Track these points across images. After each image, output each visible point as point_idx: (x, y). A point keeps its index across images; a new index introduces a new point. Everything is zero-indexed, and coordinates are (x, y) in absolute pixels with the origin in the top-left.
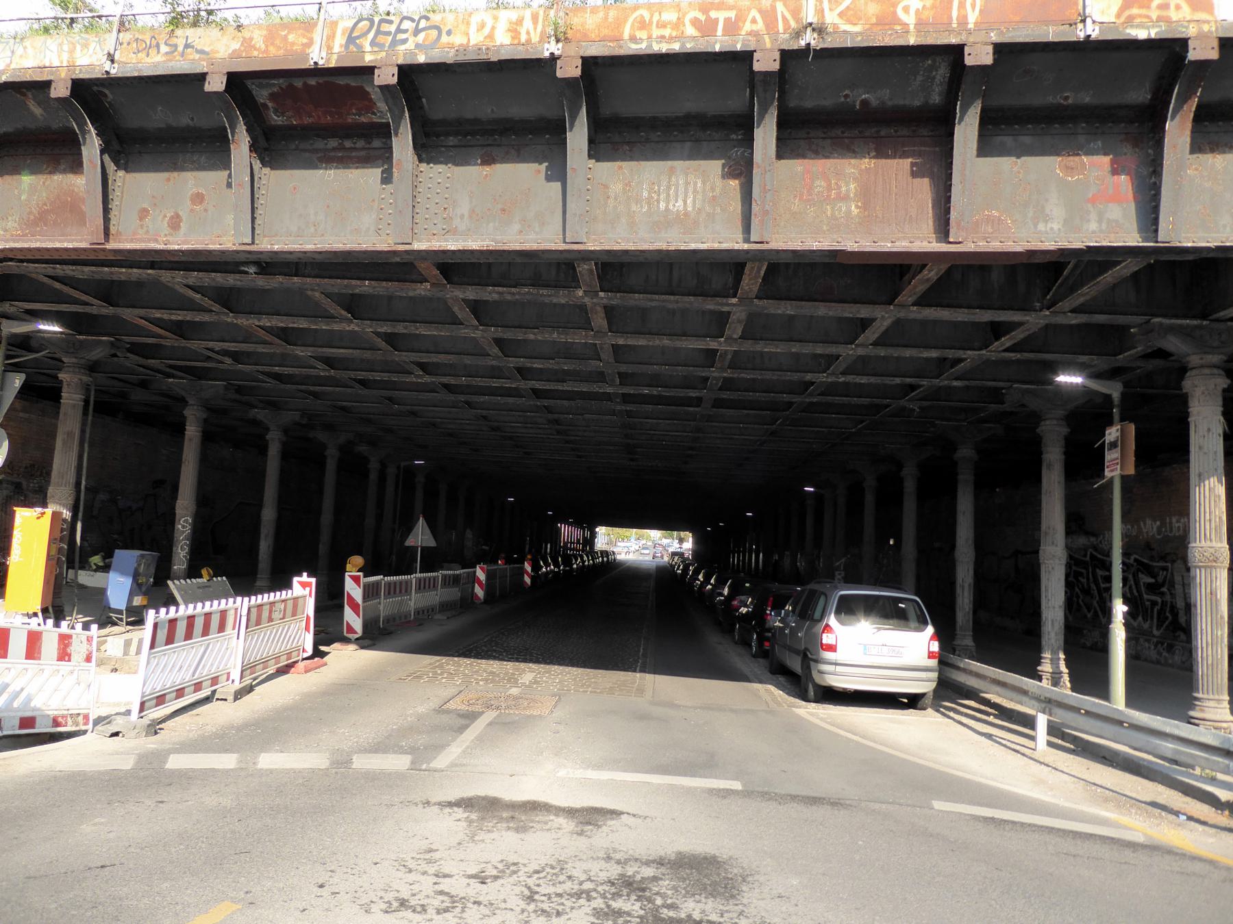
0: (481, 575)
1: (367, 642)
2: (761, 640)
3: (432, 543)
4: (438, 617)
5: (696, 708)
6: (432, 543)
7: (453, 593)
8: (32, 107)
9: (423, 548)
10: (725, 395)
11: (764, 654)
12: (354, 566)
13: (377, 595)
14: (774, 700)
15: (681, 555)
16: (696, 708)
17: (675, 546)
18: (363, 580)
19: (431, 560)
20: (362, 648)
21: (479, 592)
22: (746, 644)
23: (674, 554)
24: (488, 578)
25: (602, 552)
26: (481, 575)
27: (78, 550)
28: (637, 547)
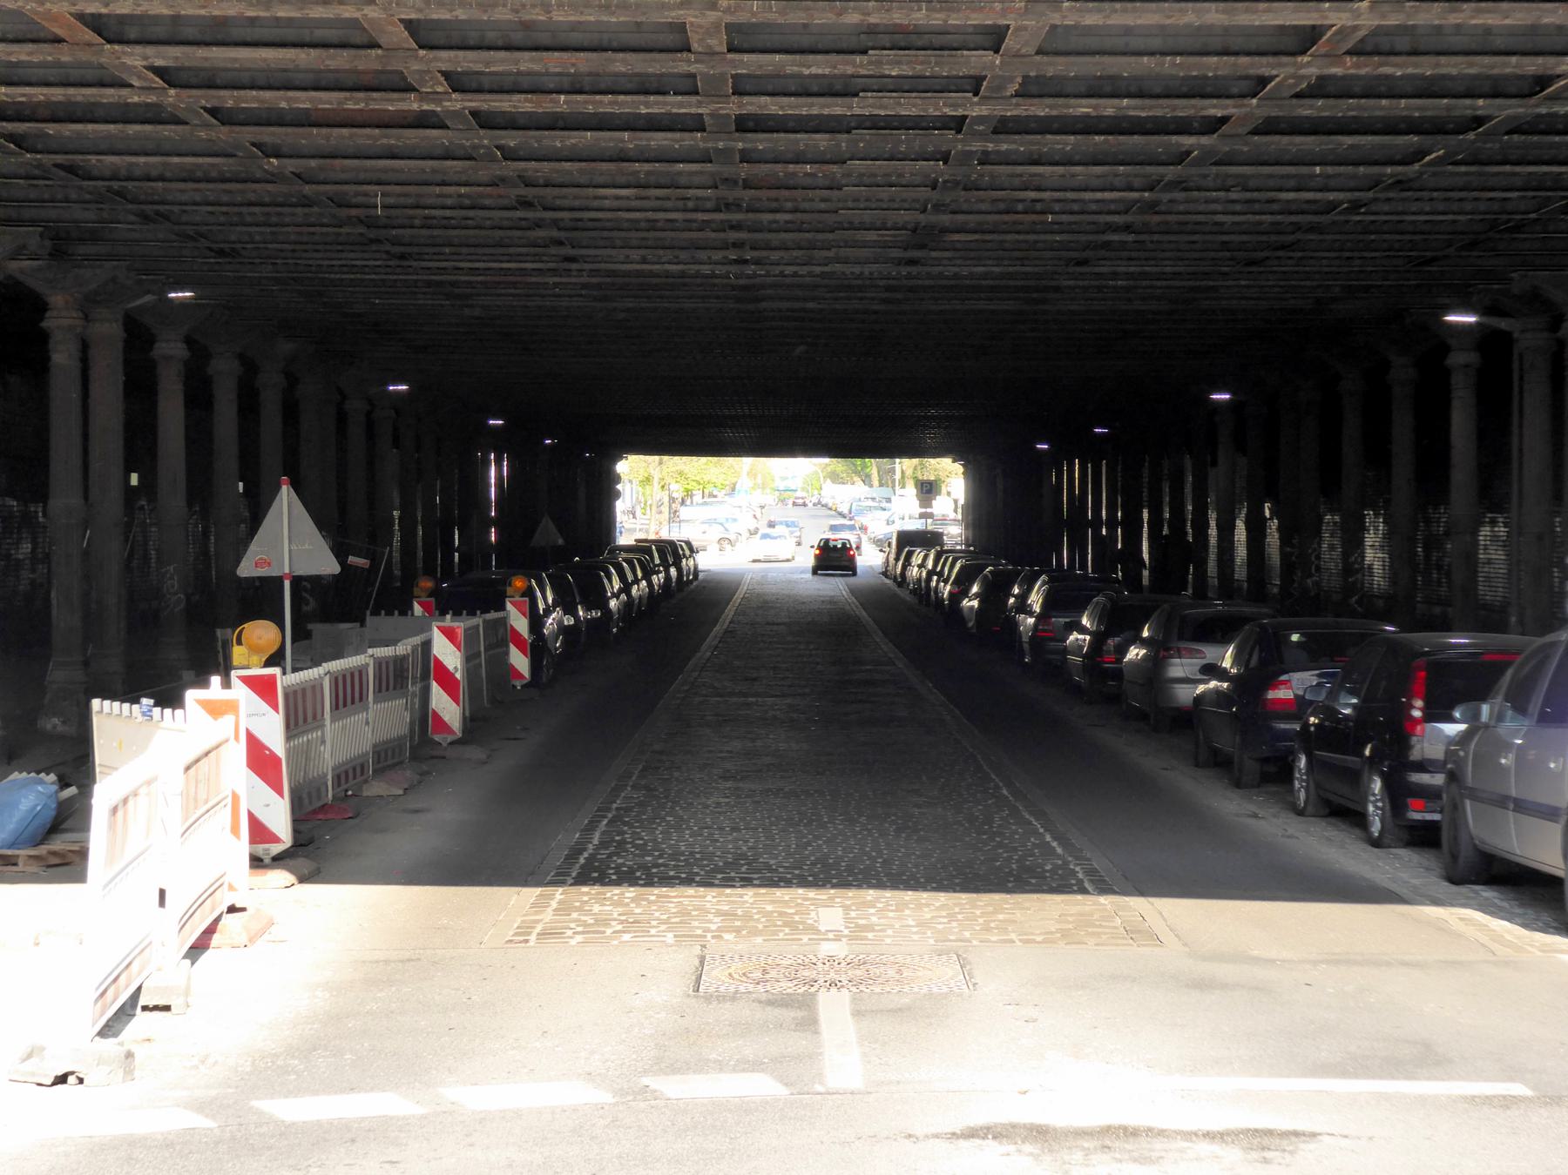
0: (448, 654)
1: (305, 864)
2: (1398, 793)
3: (325, 564)
4: (376, 788)
5: (1315, 963)
6: (325, 564)
7: (382, 720)
8: (1370, 539)
9: (297, 581)
10: (1056, 67)
11: (1424, 838)
12: (254, 649)
13: (317, 718)
14: (1498, 938)
15: (927, 539)
16: (1315, 963)
17: (905, 512)
18: (284, 680)
19: (323, 612)
20: (303, 880)
21: (446, 707)
22: (1349, 815)
23: (908, 541)
24: (470, 658)
25: (642, 548)
26: (448, 654)
27: (1026, 646)
28: (744, 518)
